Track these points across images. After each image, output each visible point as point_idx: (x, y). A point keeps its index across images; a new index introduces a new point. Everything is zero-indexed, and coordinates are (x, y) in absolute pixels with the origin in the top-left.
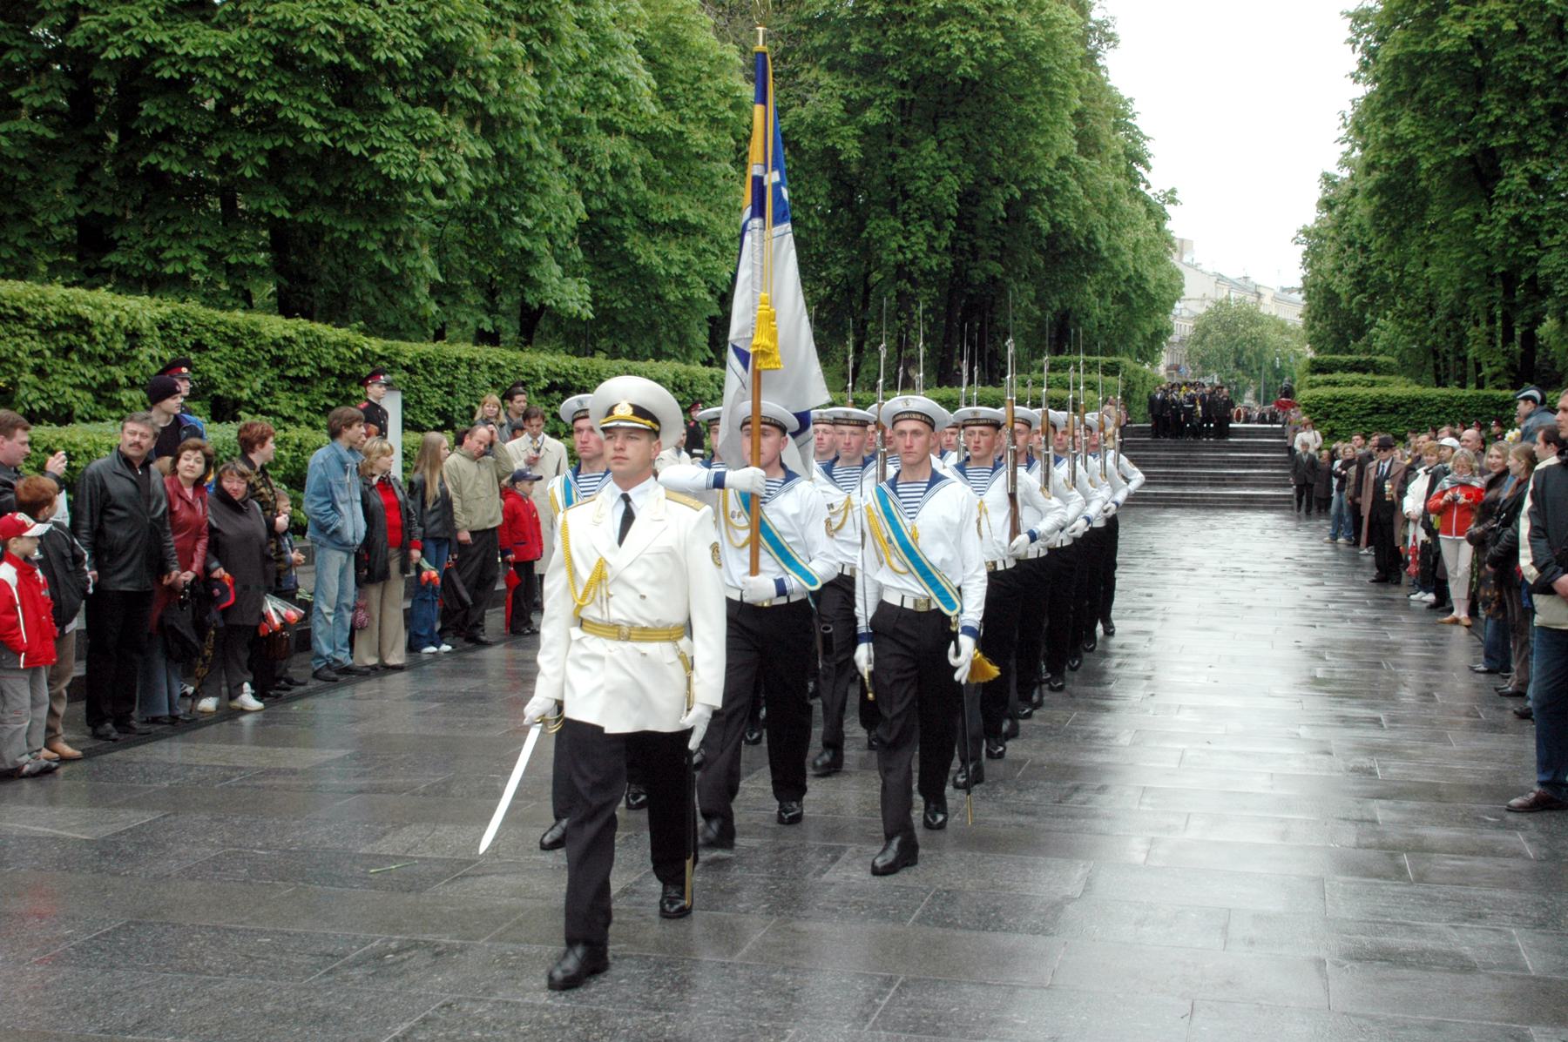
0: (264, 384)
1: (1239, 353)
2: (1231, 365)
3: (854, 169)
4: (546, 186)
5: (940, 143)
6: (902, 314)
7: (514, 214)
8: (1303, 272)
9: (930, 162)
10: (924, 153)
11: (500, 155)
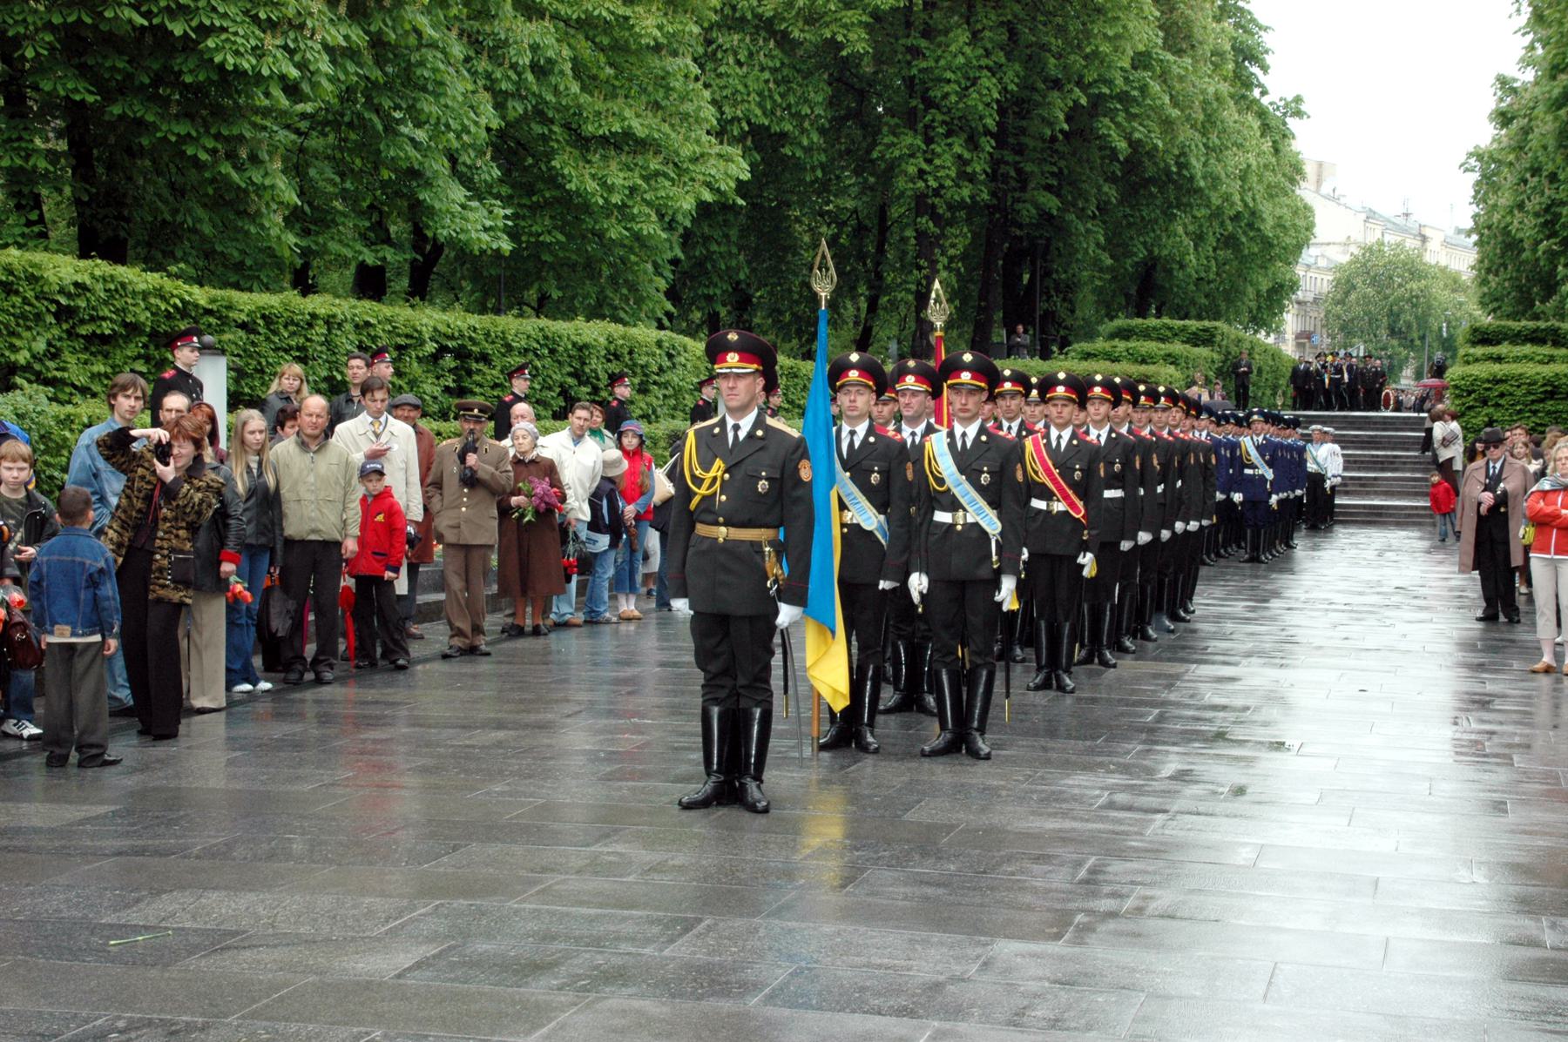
0: (49, 344)
1: (1394, 315)
2: (1383, 334)
3: (868, 68)
4: (442, 84)
5: (975, 35)
6: (922, 262)
7: (398, 122)
8: (1475, 209)
9: (961, 60)
10: (953, 48)
11: (377, 42)
